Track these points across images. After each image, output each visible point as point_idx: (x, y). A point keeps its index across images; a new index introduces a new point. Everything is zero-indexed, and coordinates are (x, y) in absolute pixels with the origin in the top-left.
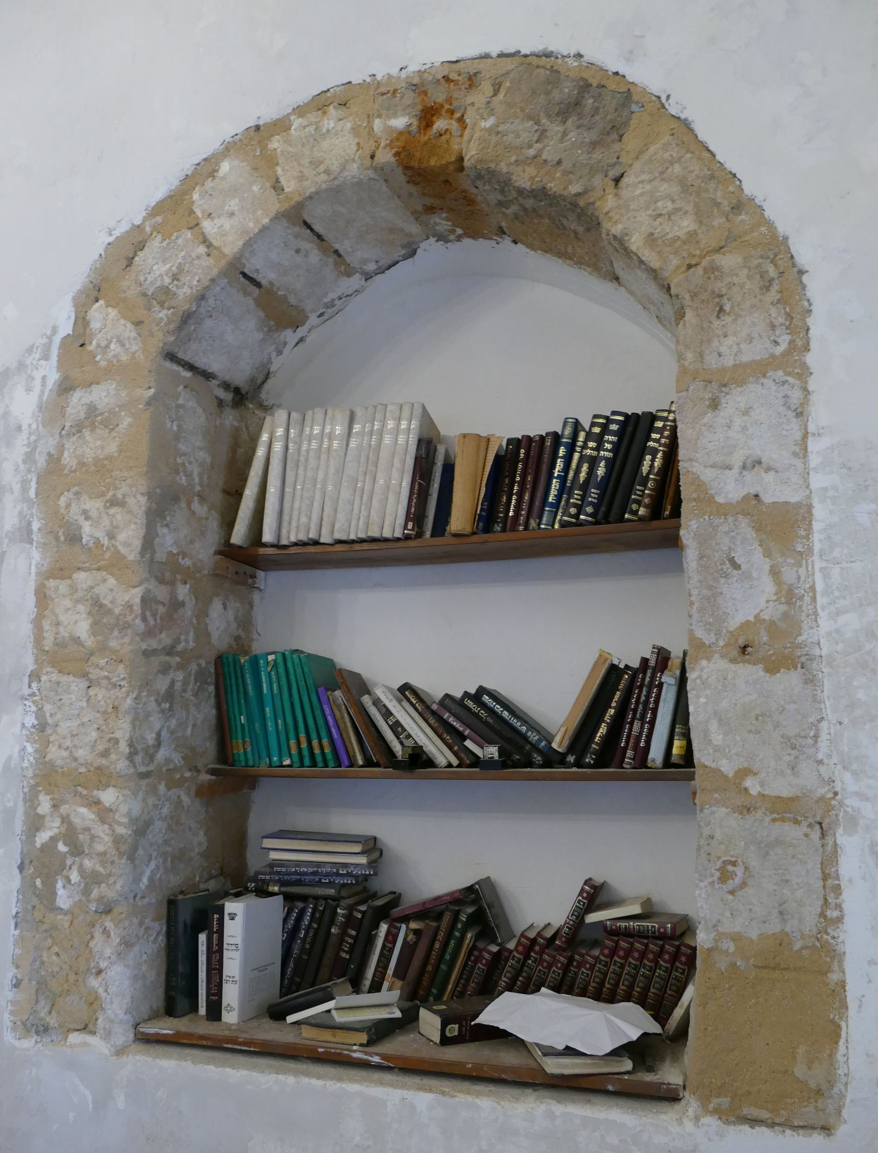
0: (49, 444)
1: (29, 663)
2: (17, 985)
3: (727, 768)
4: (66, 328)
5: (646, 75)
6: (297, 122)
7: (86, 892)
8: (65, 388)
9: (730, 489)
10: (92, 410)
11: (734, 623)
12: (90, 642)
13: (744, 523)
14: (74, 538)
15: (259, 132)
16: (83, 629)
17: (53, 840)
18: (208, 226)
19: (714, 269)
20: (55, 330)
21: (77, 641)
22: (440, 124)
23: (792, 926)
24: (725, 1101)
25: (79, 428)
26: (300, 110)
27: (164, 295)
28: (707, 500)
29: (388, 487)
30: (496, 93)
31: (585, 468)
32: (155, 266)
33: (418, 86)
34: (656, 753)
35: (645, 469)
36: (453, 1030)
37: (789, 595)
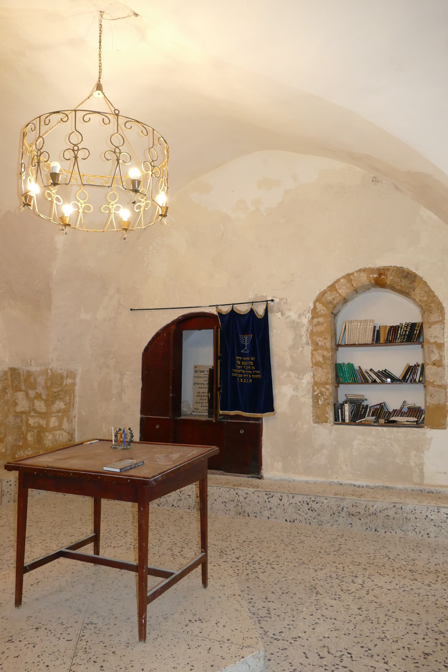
0: (311, 328)
1: (311, 365)
2: (313, 416)
3: (431, 381)
4: (312, 307)
5: (419, 273)
6: (355, 274)
7: (325, 401)
8: (313, 318)
9: (432, 340)
10: (318, 322)
11: (433, 360)
12: (322, 362)
13: (434, 345)
14: (317, 344)
15: (349, 275)
16: (321, 360)
17: (318, 394)
18: (339, 290)
19: (430, 306)
20: (310, 308)
21: (320, 361)
22: (383, 277)
23: (441, 402)
24: (430, 426)
25: (316, 325)
26: (356, 272)
27: (331, 303)
28: (429, 342)
29: (369, 335)
30: (393, 272)
31: (404, 332)
32: (329, 297)
33: (379, 269)
34: (417, 380)
35: (415, 333)
36: (386, 421)
37: (441, 356)
